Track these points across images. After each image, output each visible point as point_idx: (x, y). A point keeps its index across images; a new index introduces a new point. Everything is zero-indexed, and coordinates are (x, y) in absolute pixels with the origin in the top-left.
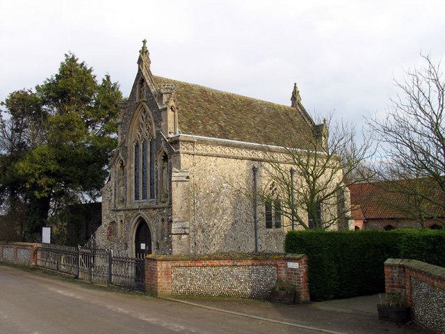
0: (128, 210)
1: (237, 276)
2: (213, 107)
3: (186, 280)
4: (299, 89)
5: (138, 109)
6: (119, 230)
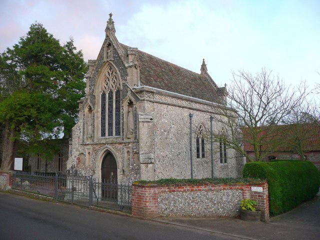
0: (96, 144)
1: (212, 199)
2: (158, 70)
3: (170, 203)
4: (206, 63)
6: (87, 160)
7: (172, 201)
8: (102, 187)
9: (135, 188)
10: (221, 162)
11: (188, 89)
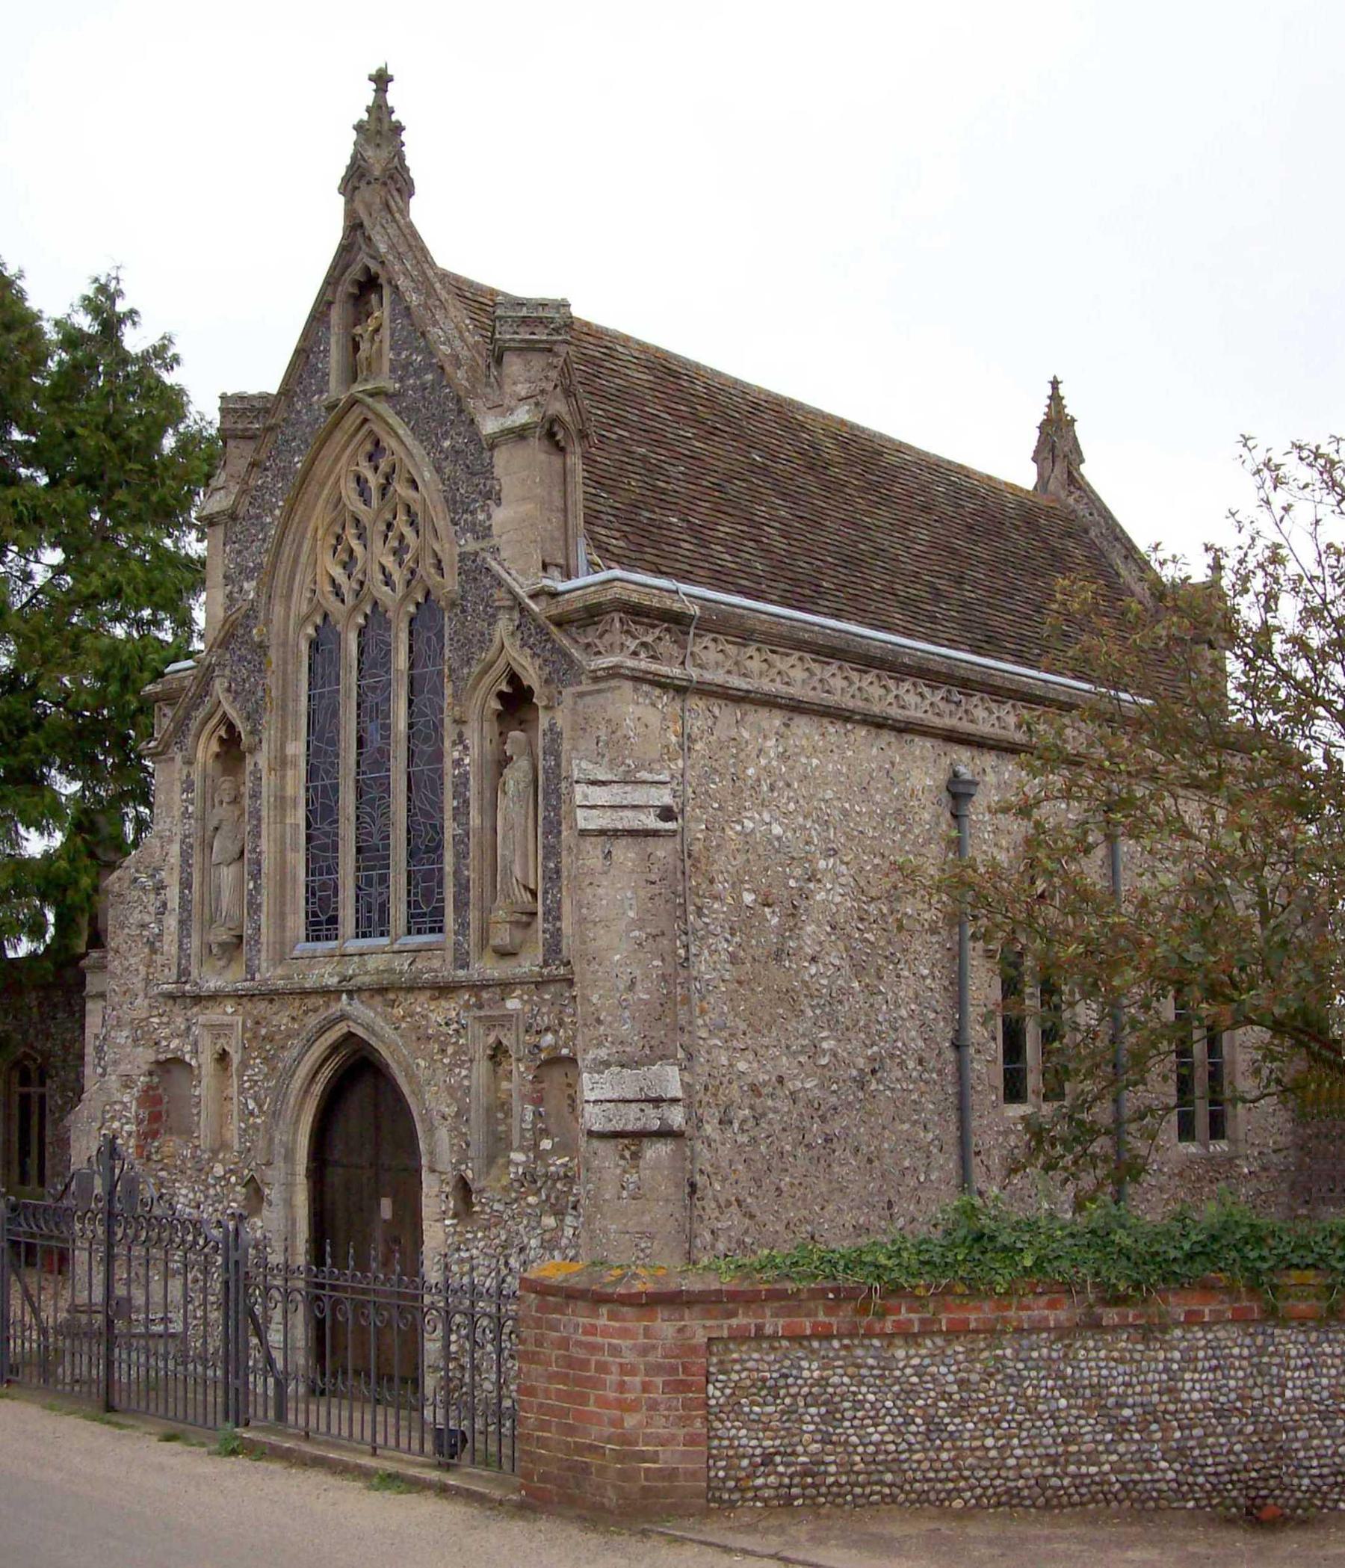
0: (271, 995)
1: (1099, 1390)
5: (339, 437)
7: (812, 1400)
8: (314, 1301)
9: (542, 1308)
10: (1186, 1132)
11: (937, 595)
